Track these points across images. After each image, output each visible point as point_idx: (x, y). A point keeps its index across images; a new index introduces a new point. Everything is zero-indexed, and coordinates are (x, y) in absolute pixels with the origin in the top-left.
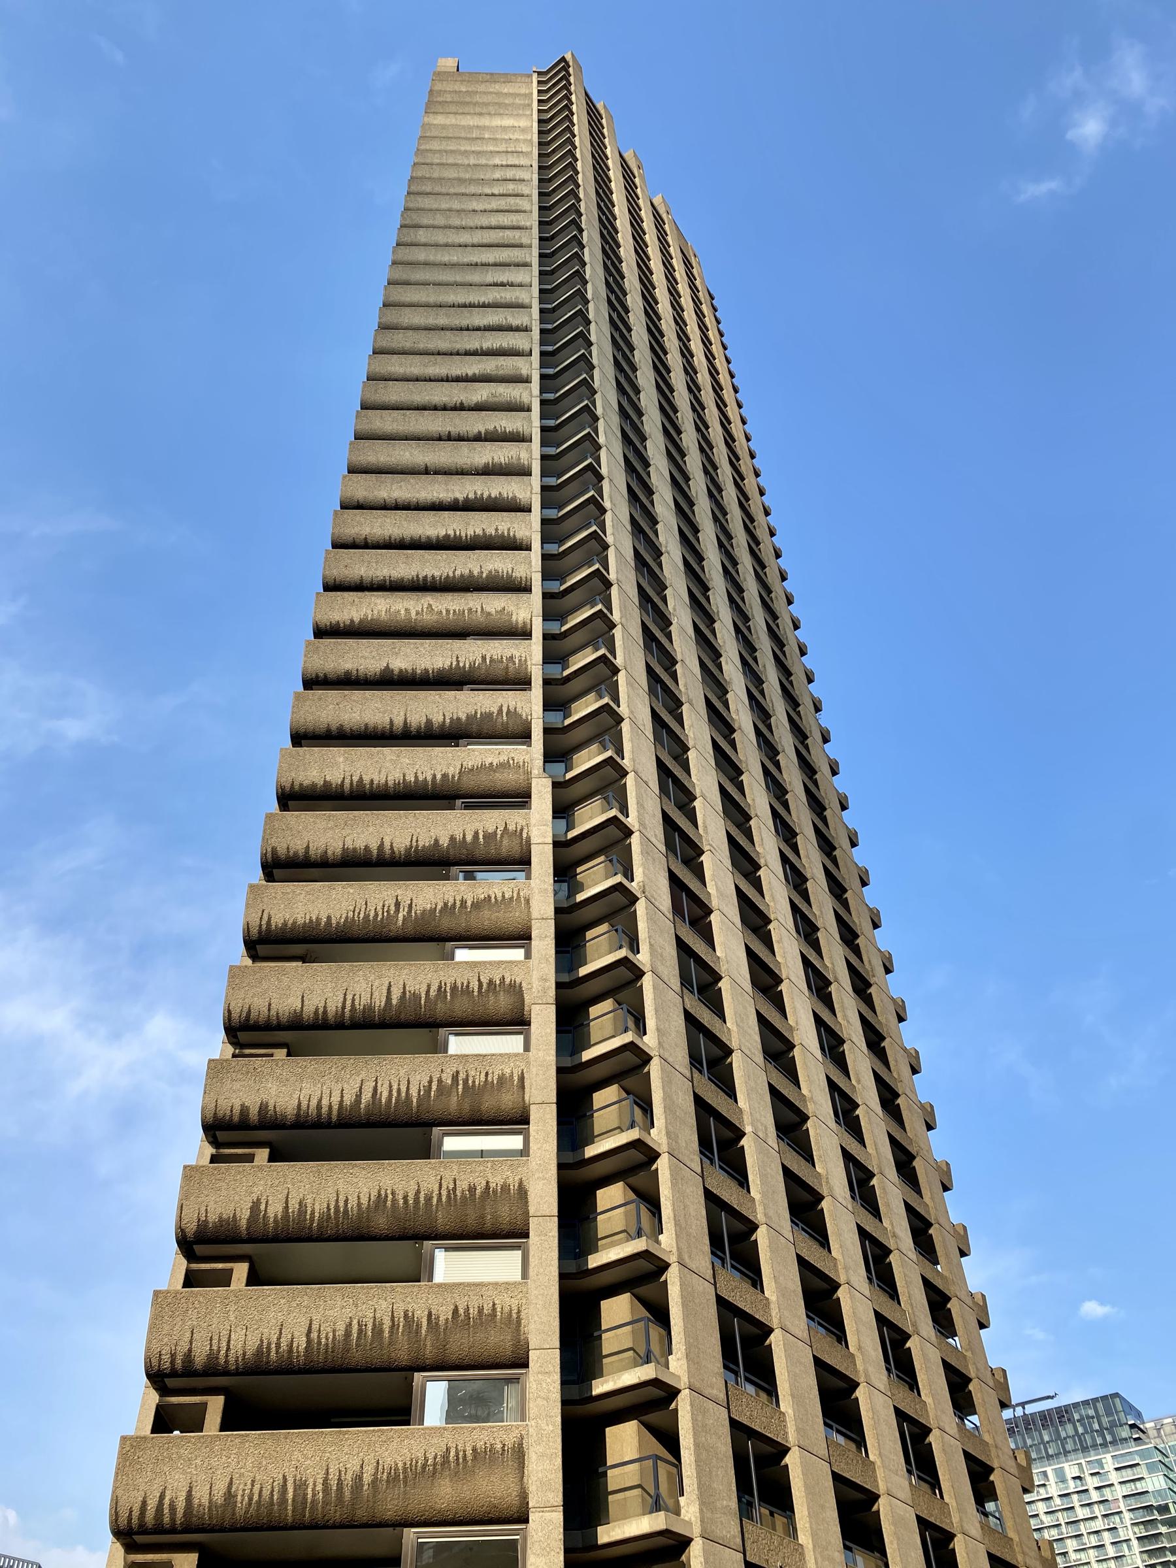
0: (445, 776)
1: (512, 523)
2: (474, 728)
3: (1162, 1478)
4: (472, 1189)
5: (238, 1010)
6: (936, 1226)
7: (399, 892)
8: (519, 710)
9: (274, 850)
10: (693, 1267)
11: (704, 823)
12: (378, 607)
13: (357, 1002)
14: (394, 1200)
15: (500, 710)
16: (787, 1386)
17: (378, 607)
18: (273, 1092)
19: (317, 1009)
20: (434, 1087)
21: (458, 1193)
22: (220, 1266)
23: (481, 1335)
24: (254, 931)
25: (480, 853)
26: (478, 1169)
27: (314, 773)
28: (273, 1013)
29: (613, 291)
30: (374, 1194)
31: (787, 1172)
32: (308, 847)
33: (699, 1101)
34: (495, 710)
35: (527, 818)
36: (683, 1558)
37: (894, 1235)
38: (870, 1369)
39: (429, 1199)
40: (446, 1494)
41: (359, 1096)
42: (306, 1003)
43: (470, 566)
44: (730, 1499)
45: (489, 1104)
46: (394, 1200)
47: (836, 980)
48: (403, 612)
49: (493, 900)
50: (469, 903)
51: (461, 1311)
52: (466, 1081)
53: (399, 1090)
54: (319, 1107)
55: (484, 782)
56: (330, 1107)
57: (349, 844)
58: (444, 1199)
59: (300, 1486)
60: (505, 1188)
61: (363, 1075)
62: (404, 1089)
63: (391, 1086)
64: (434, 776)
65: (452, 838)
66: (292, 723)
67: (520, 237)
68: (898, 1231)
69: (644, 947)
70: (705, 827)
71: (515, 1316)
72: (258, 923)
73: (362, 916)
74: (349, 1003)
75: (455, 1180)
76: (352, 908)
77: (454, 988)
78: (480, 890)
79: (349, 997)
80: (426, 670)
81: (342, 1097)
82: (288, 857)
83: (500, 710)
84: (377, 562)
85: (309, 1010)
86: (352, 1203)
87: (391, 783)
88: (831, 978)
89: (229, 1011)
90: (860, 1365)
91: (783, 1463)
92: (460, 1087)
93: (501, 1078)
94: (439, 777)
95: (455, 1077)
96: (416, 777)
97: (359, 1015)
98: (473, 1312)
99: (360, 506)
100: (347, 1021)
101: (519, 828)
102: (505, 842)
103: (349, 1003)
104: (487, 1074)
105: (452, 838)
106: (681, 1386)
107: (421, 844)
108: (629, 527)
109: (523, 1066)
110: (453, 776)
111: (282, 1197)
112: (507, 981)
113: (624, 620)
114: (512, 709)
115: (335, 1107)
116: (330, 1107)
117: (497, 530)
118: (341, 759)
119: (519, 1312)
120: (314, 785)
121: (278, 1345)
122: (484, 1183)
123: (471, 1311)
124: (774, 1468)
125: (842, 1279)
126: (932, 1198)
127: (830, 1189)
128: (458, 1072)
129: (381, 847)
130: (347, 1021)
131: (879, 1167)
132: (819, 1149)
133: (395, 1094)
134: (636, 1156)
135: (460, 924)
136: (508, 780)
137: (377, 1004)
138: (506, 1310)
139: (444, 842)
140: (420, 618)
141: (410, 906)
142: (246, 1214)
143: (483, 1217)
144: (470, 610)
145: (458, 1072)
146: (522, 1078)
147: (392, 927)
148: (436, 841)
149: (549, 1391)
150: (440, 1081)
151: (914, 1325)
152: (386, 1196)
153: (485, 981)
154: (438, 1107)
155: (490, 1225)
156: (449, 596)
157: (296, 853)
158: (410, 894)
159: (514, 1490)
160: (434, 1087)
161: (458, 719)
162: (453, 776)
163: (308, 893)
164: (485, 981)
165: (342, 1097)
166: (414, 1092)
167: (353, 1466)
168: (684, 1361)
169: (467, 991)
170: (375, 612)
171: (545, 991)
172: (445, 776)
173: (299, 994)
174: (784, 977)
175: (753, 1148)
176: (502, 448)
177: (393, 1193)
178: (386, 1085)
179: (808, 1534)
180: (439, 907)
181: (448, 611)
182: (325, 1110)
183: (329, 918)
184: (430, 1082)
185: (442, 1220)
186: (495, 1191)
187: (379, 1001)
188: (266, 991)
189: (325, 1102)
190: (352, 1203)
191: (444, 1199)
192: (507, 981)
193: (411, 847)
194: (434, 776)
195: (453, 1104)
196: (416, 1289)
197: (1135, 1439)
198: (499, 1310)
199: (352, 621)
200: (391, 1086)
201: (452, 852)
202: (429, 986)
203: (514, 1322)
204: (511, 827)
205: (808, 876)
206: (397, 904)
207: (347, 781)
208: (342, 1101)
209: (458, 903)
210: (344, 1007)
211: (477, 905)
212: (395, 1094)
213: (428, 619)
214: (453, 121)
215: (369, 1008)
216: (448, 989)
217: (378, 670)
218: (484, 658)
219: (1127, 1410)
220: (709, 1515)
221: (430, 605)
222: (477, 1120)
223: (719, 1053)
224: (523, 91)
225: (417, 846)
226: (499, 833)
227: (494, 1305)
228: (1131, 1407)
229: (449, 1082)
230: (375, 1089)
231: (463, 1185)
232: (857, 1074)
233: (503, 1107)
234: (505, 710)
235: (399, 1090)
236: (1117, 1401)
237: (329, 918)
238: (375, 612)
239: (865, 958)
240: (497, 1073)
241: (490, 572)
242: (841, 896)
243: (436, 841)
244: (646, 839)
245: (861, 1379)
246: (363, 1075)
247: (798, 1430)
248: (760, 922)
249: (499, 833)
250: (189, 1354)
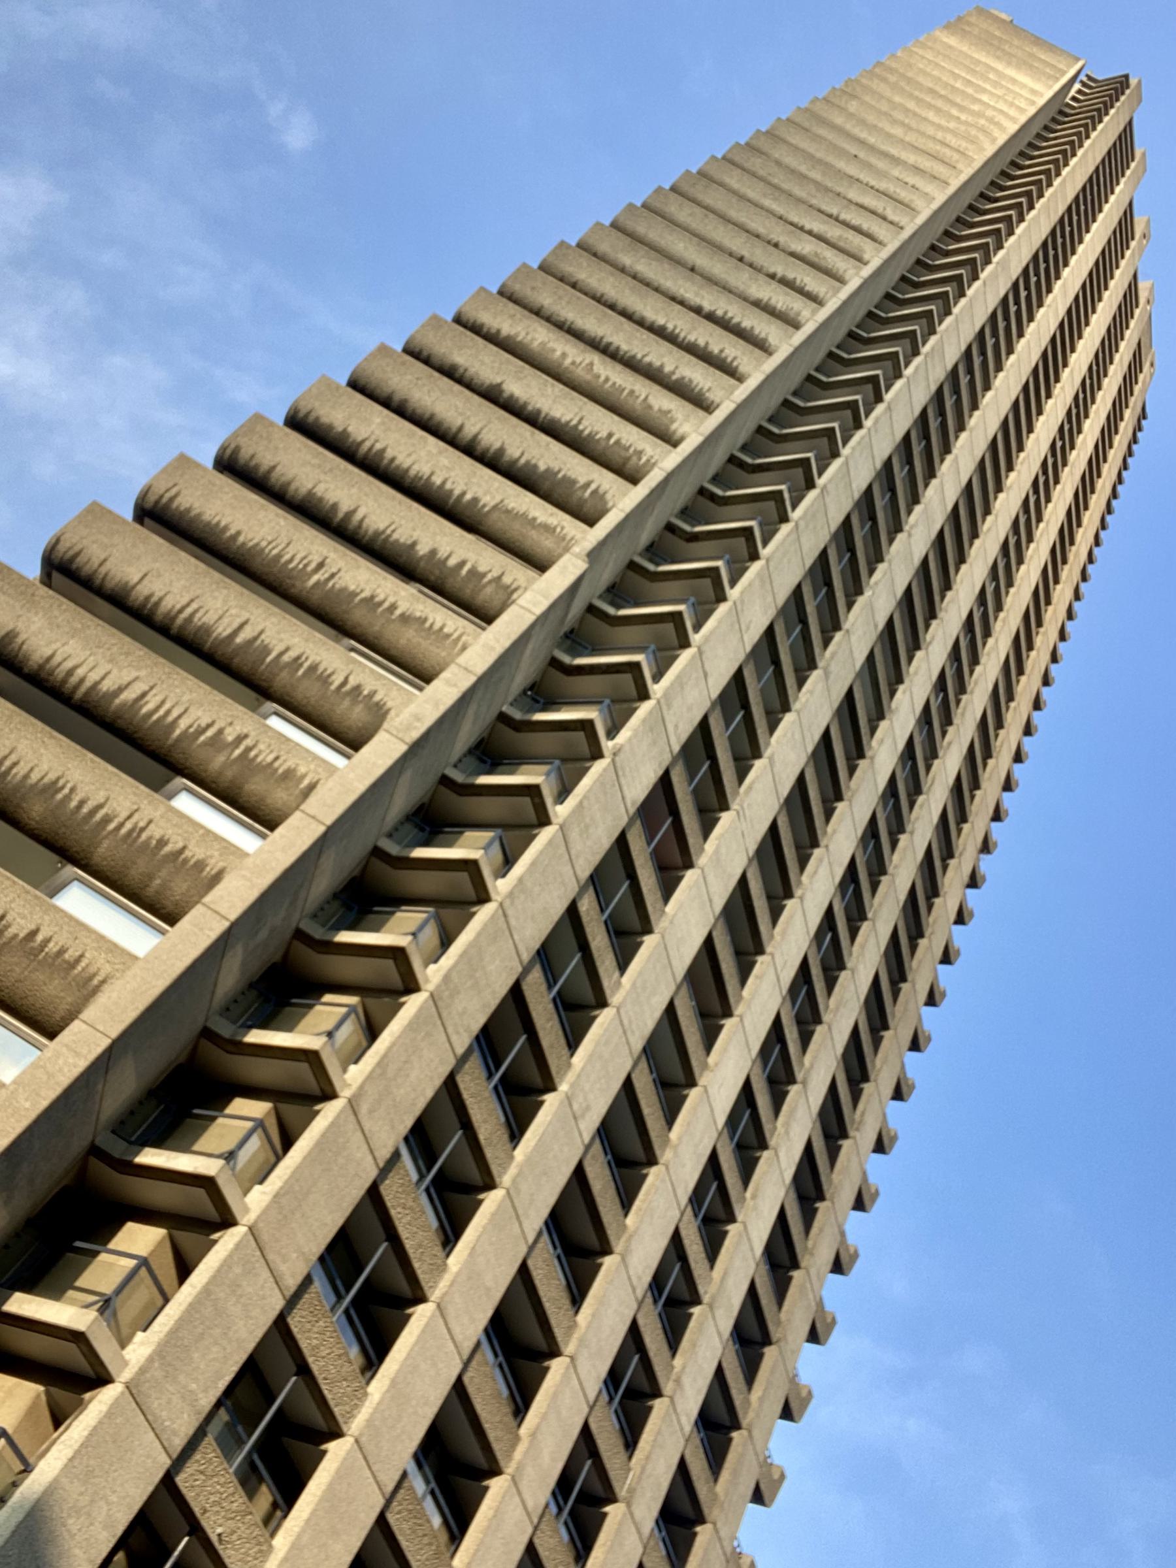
0: (475, 500)
1: (744, 354)
2: (546, 486)
4: (162, 842)
5: (68, 545)
6: (744, 1432)
7: (332, 555)
8: (608, 496)
9: (237, 450)
10: (367, 1126)
11: (753, 782)
12: (538, 336)
13: (198, 615)
14: (68, 798)
15: (588, 485)
17: (538, 336)
18: (34, 628)
19: (151, 595)
20: (209, 733)
21: (144, 836)
23: (40, 976)
24: (152, 498)
25: (451, 584)
26: (185, 827)
27: (340, 416)
28: (103, 570)
29: (1054, 455)
30: (52, 776)
31: (682, 1467)
32: (274, 467)
33: (634, 1330)
34: (582, 480)
35: (530, 582)
36: (87, 1396)
37: (678, 1381)
38: (529, 1471)
39: (107, 820)
41: (121, 690)
42: (145, 582)
43: (665, 360)
44: (205, 1391)
45: (255, 787)
46: (68, 798)
47: (804, 1083)
48: (558, 353)
49: (427, 625)
50: (398, 612)
51: (40, 938)
52: (249, 749)
53: (168, 712)
54: (70, 673)
55: (515, 531)
56: (82, 681)
57: (319, 491)
58: (124, 831)
60: (200, 865)
61: (143, 673)
62: (175, 714)
63: (163, 702)
64: (464, 494)
65: (433, 552)
66: (357, 367)
67: (957, 161)
68: (686, 1381)
69: (572, 801)
70: (750, 788)
71: (95, 982)
72: (161, 492)
73: (275, 552)
74: (189, 610)
75: (150, 822)
76: (270, 538)
77: (313, 668)
78: (421, 607)
79: (194, 606)
80: (539, 412)
81: (103, 678)
82: (246, 465)
83: (588, 485)
84: (568, 303)
85: (142, 591)
87: (412, 473)
88: (799, 1076)
90: (518, 1454)
91: (323, 1447)
92: (237, 752)
94: (468, 497)
95: (240, 739)
96: (444, 483)
97: (191, 629)
98: (52, 947)
99: (476, 329)
100: (174, 631)
101: (513, 587)
102: (489, 590)
103: (189, 610)
104: (277, 758)
105: (433, 552)
107: (395, 536)
108: (879, 465)
109: (323, 775)
110: (484, 506)
112: (377, 698)
113: (802, 524)
114: (601, 491)
115: (88, 684)
116: (82, 681)
117: (722, 351)
118: (378, 420)
119: (103, 982)
120: (330, 427)
122: (180, 845)
123: (51, 945)
124: (311, 1446)
125: (569, 1348)
126: (761, 1400)
128: (246, 736)
129: (350, 514)
130: (174, 631)
131: (713, 1298)
132: (643, 1201)
133: (161, 712)
134: (388, 969)
135: (374, 625)
136: (542, 544)
137: (220, 630)
138: (92, 970)
139: (422, 549)
140: (572, 368)
141: (333, 576)
143: (151, 877)
144: (632, 392)
145: (246, 736)
146: (312, 787)
147: (298, 583)
148: (414, 544)
149: (61, 1070)
150: (221, 731)
151: (632, 1491)
152: (63, 788)
153: (352, 682)
154: (197, 754)
155: (156, 900)
156: (635, 430)
157: (257, 466)
158: (341, 564)
159: (63, 1008)
160: (209, 733)
161: (535, 466)
162: (484, 506)
163: (235, 497)
165: (103, 678)
166: (183, 724)
169: (325, 680)
170: (529, 337)
171: (409, 728)
172: (475, 500)
173: (144, 570)
175: (554, 1109)
176: (787, 294)
177: (72, 790)
178: (159, 698)
179: (291, 1539)
180: (363, 595)
181: (607, 380)
182: (74, 680)
183: (239, 533)
184: (209, 726)
185: (103, 851)
186: (186, 861)
187: (223, 630)
188: (113, 545)
189: (80, 672)
190: (20, 770)
191: (124, 831)
192: (377, 698)
193: (383, 532)
194: (464, 494)
195: (217, 763)
196: (7, 883)
198: (83, 964)
199: (499, 331)
200: (163, 702)
201: (422, 564)
202: (287, 649)
204: (507, 580)
205: (849, 965)
206: (321, 565)
207: (367, 445)
208: (97, 683)
209: (386, 605)
210: (181, 611)
211: (405, 619)
212: (161, 712)
213: (580, 373)
214: (965, 49)
215: (207, 630)
216: (306, 665)
217: (488, 382)
218: (610, 435)
220: (159, 1374)
221: (591, 364)
222: (231, 796)
223: (686, 1296)
224: (1061, 66)
225: (390, 536)
226: (489, 577)
227: (82, 956)
229: (230, 739)
230: (144, 695)
231: (155, 832)
232: (756, 1189)
233: (269, 801)
234: (593, 487)
235: (168, 712)
237: (239, 533)
238: (529, 337)
239: (861, 1106)
240: (290, 763)
241: (683, 378)
242: (878, 1031)
243: (414, 544)
245: (510, 1469)
247: (370, 1422)
248: (751, 947)
249: (489, 577)
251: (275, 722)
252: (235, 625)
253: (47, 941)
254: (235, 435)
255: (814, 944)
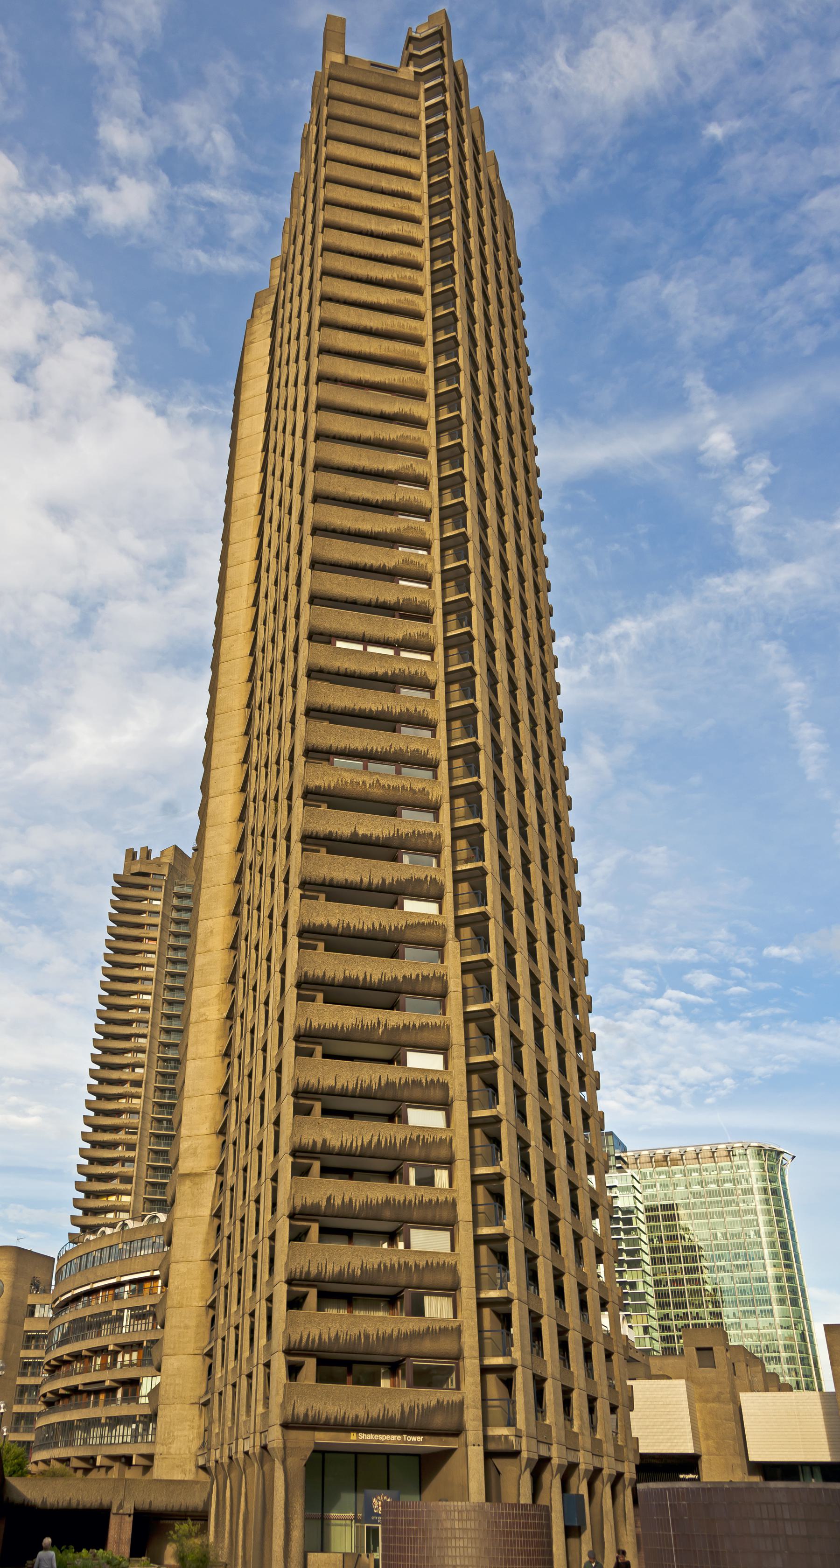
3: (632, 1199)
4: (430, 1201)
6: (597, 1162)
16: (544, 1286)
22: (305, 1224)
28: (321, 1087)
30: (384, 1199)
34: (423, 878)
40: (427, 1346)
52: (423, 1140)
56: (357, 1146)
59: (367, 1337)
61: (373, 1131)
65: (404, 977)
77: (413, 1081)
86: (374, 1202)
89: (298, 1083)
93: (441, 1139)
95: (418, 1137)
105: (404, 977)
106: (514, 1298)
111: (341, 1197)
112: (441, 1081)
116: (357, 1146)
121: (348, 1272)
127: (560, 1163)
142: (324, 1204)
159: (456, 1347)
164: (428, 1080)
167: (389, 1331)
168: (516, 1287)
171: (461, 1092)
174: (545, 1023)
190: (374, 1202)
197: (618, 1168)
203: (453, 1270)
204: (438, 975)
206: (379, 1023)
219: (616, 1145)
221: (378, 781)
228: (620, 1143)
230: (379, 1139)
236: (610, 1138)
244: (499, 969)
246: (373, 1131)
250: (308, 1272)
251: (401, 582)
252: (377, 1079)
253: (432, 1263)
254: (286, 1270)
255: (500, 842)
